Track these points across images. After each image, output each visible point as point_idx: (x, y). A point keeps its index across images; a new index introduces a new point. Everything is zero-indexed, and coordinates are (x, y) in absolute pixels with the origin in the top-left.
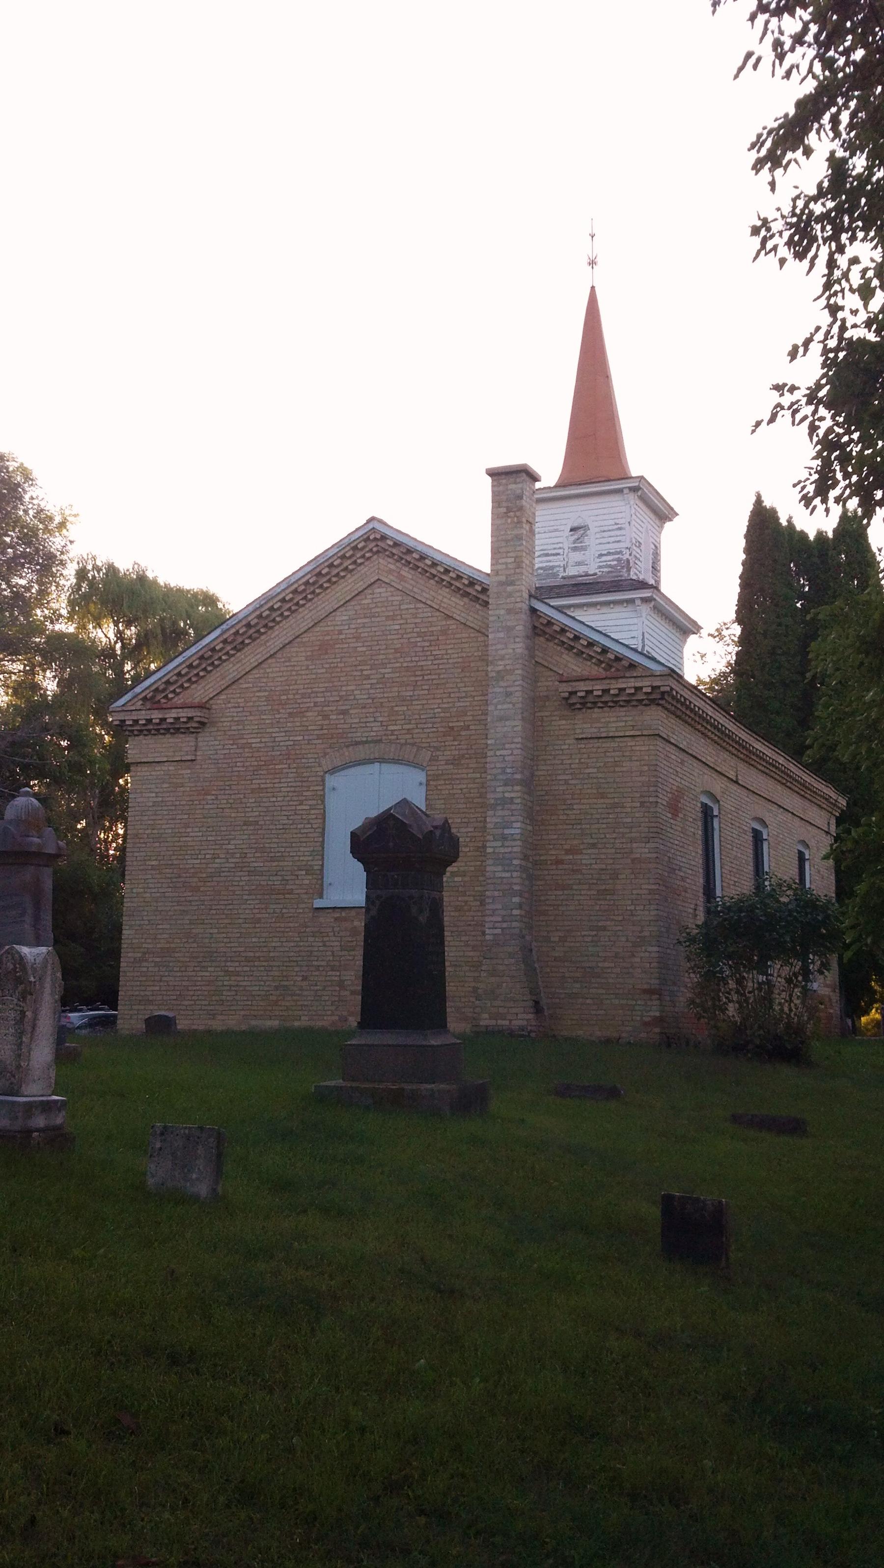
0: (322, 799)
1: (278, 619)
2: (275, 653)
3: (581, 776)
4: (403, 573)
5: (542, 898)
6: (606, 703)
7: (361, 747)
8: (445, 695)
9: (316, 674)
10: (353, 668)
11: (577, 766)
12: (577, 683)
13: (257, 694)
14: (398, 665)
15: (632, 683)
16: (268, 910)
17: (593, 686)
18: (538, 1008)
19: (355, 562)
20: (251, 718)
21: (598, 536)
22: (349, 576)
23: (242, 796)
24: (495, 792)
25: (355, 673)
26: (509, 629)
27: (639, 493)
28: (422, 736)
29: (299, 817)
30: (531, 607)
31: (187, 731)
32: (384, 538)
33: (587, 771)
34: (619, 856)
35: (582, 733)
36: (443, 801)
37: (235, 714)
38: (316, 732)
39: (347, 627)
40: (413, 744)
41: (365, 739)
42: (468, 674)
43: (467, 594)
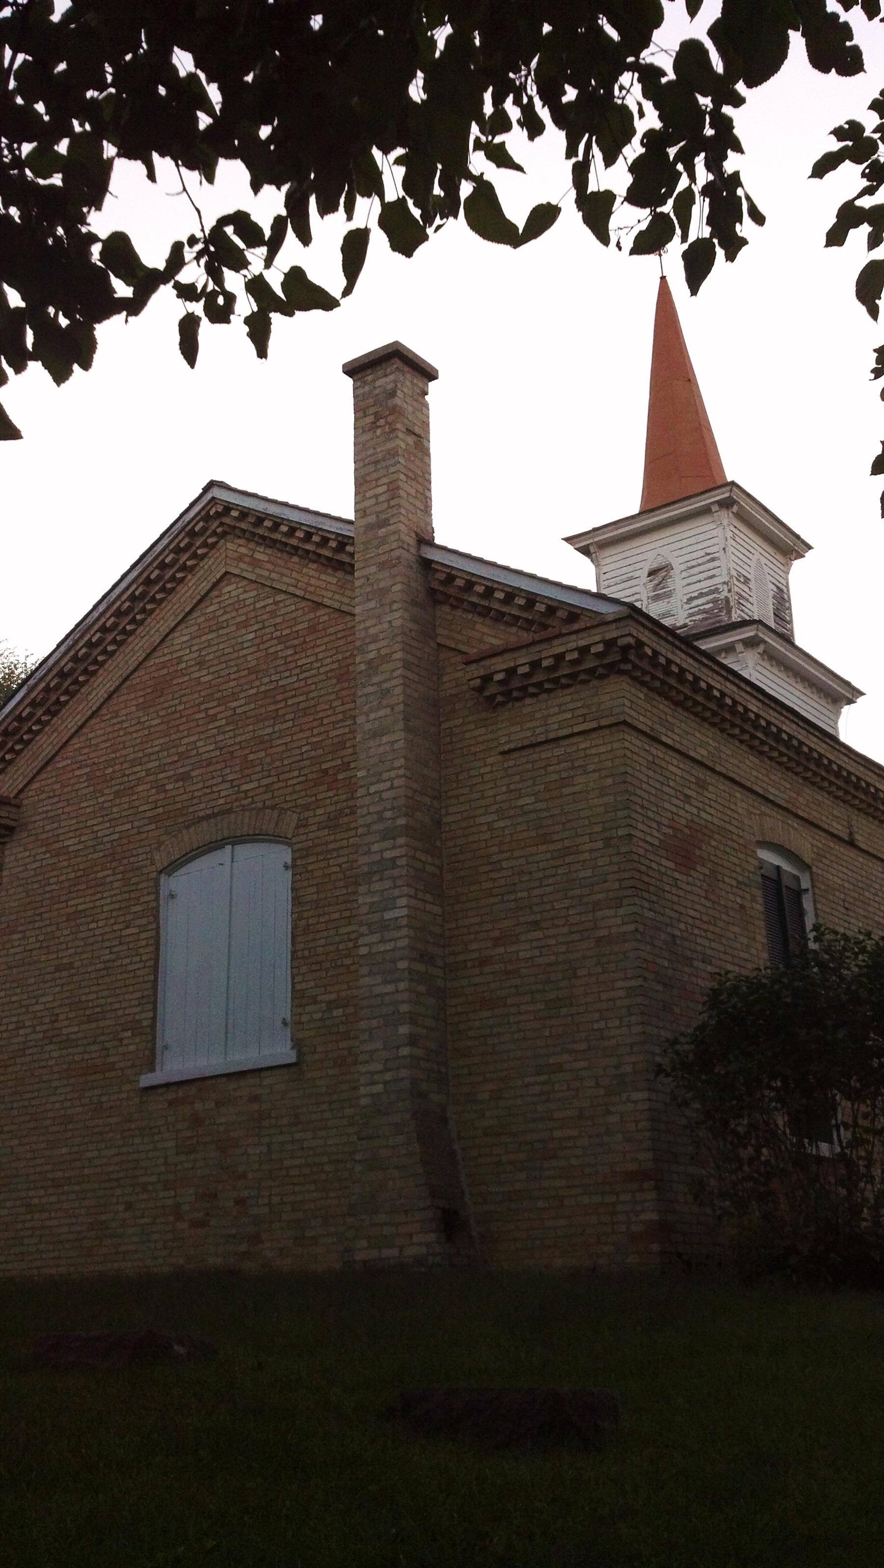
0: (155, 914)
1: (100, 658)
2: (99, 708)
3: (512, 813)
4: (258, 556)
5: (462, 1027)
6: (539, 685)
7: (204, 824)
8: (315, 724)
10: (196, 709)
11: (504, 797)
15: (576, 642)
16: (83, 1101)
18: (450, 1223)
19: (194, 556)
21: (684, 574)
23: (54, 928)
24: (368, 853)
25: (197, 716)
27: (735, 509)
28: (286, 791)
29: (125, 947)
30: (421, 557)
32: (228, 508)
33: (521, 802)
34: (575, 937)
36: (314, 889)
40: (273, 807)
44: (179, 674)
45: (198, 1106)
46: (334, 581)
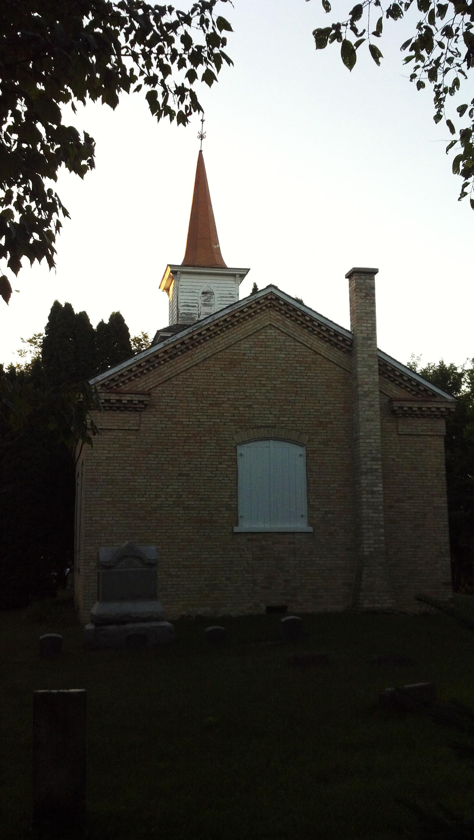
0: (236, 461)
4: (286, 322)
7: (262, 429)
8: (316, 401)
9: (228, 379)
12: (403, 402)
13: (185, 389)
14: (284, 380)
17: (413, 404)
20: (182, 404)
22: (250, 319)
23: (177, 456)
26: (371, 367)
31: (135, 410)
35: (402, 431)
37: (169, 401)
38: (229, 418)
39: (249, 352)
40: (297, 430)
41: (264, 425)
42: (330, 390)
43: (330, 341)
44: (244, 360)
45: (263, 543)
46: (326, 346)
